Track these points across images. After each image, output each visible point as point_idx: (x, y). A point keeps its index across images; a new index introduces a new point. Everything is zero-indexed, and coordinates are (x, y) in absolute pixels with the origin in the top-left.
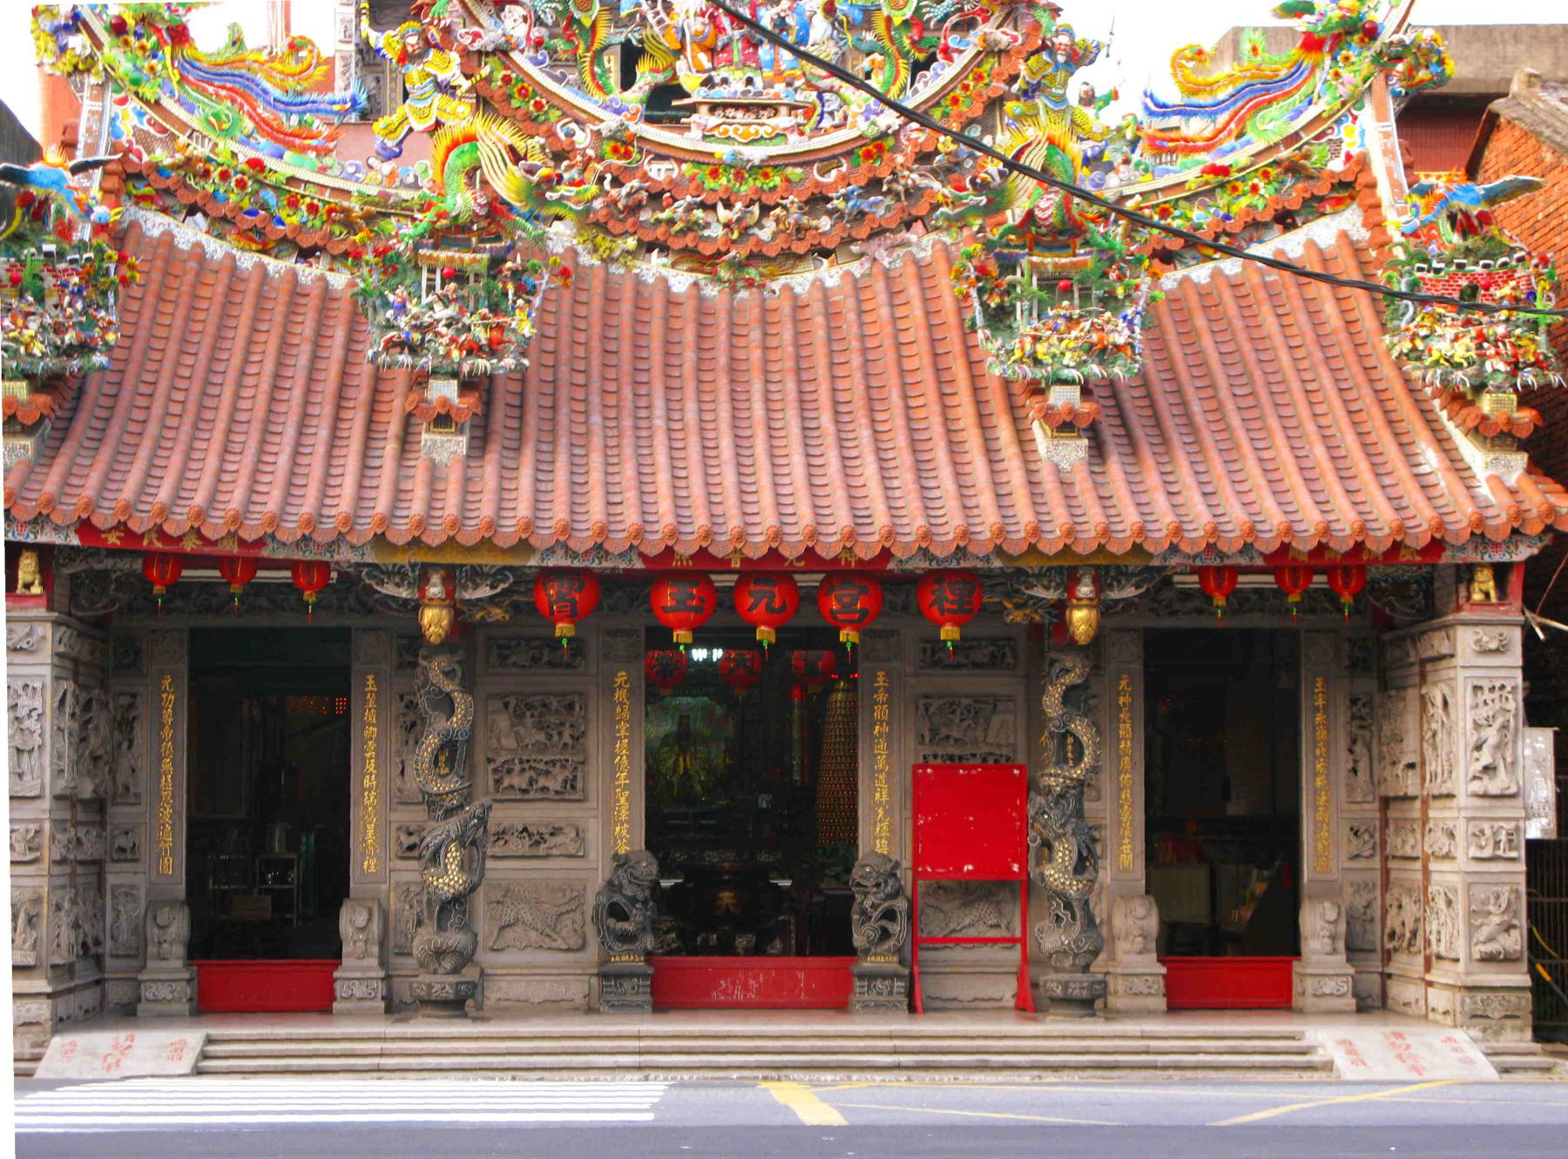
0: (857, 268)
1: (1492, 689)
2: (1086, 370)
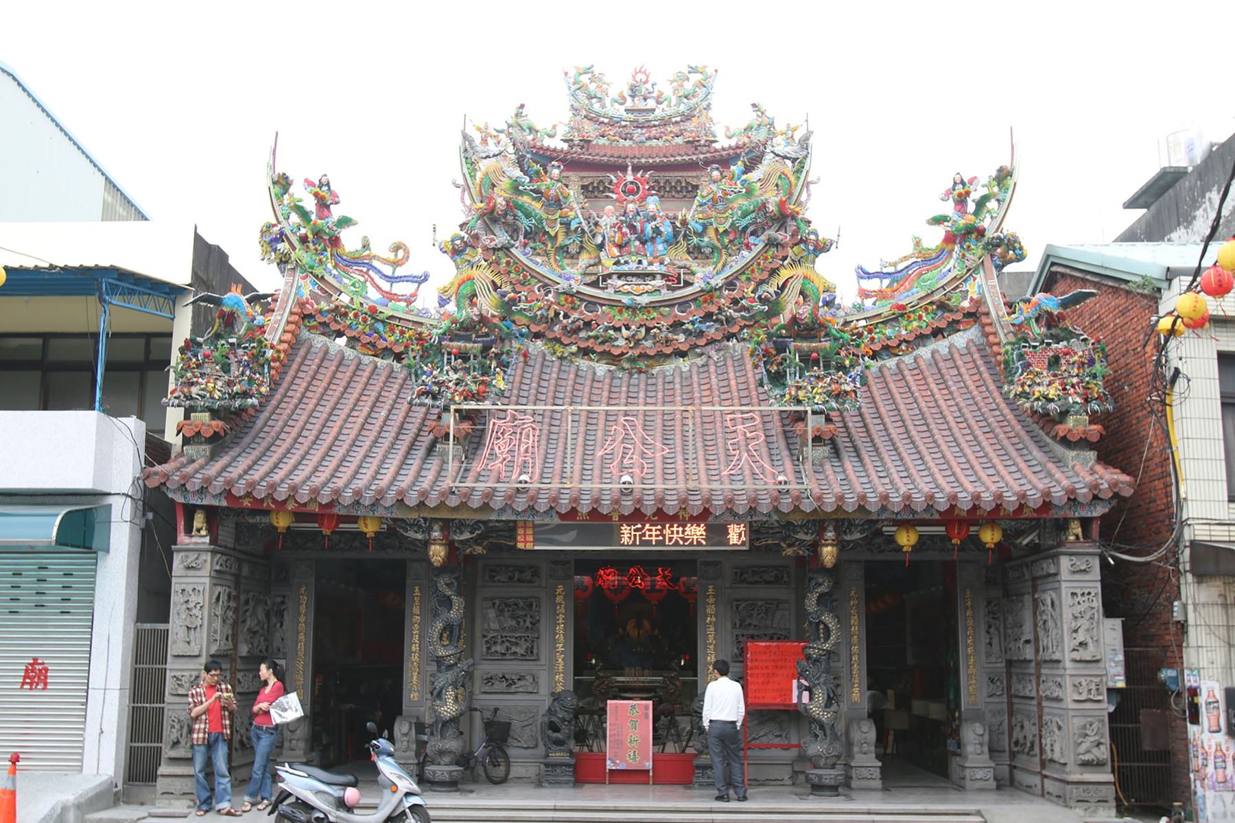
0: (699, 361)
1: (1083, 594)
2: (828, 406)
